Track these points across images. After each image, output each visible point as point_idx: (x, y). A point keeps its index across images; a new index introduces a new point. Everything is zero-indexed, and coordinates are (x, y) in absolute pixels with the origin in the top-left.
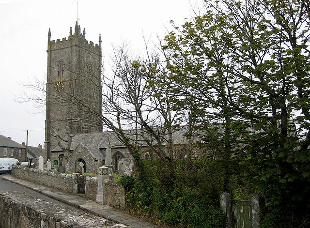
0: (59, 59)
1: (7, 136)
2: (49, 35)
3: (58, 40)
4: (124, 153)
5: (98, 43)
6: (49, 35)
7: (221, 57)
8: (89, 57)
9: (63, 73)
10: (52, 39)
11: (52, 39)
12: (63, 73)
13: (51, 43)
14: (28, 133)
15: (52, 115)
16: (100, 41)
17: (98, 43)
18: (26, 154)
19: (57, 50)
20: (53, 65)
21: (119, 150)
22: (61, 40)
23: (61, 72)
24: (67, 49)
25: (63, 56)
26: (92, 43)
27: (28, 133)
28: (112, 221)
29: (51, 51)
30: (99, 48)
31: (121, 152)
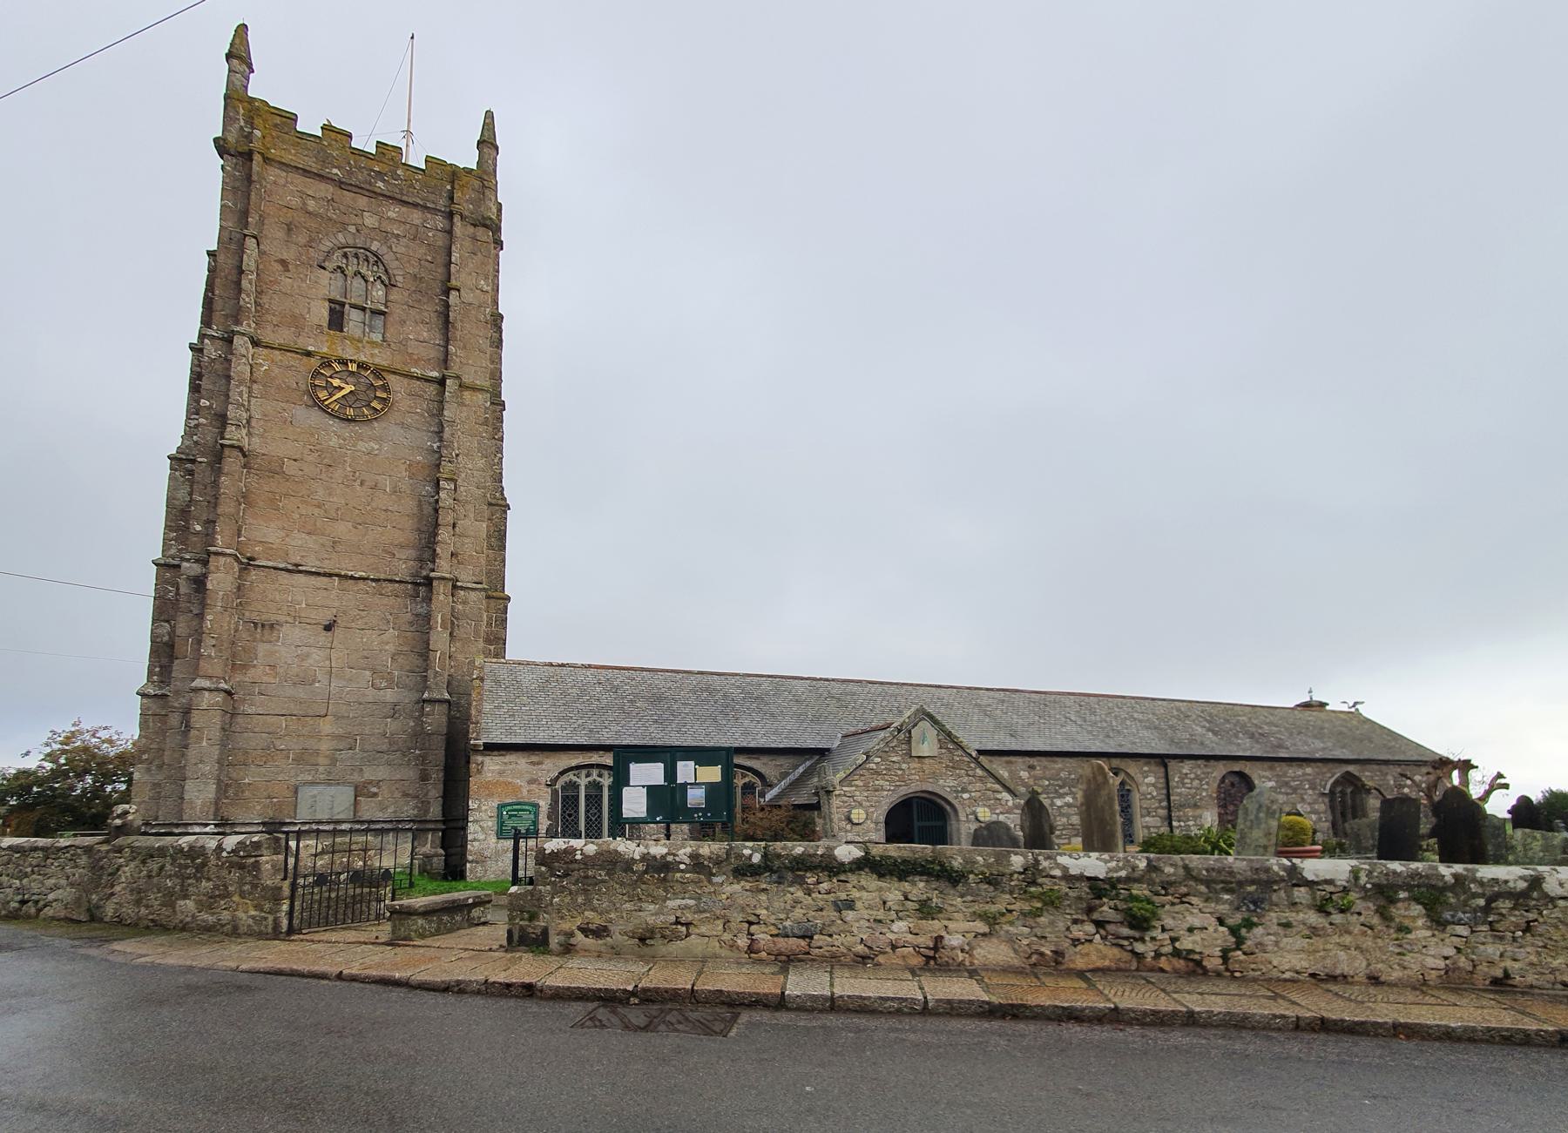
2: (239, 55)
21: (1351, 768)
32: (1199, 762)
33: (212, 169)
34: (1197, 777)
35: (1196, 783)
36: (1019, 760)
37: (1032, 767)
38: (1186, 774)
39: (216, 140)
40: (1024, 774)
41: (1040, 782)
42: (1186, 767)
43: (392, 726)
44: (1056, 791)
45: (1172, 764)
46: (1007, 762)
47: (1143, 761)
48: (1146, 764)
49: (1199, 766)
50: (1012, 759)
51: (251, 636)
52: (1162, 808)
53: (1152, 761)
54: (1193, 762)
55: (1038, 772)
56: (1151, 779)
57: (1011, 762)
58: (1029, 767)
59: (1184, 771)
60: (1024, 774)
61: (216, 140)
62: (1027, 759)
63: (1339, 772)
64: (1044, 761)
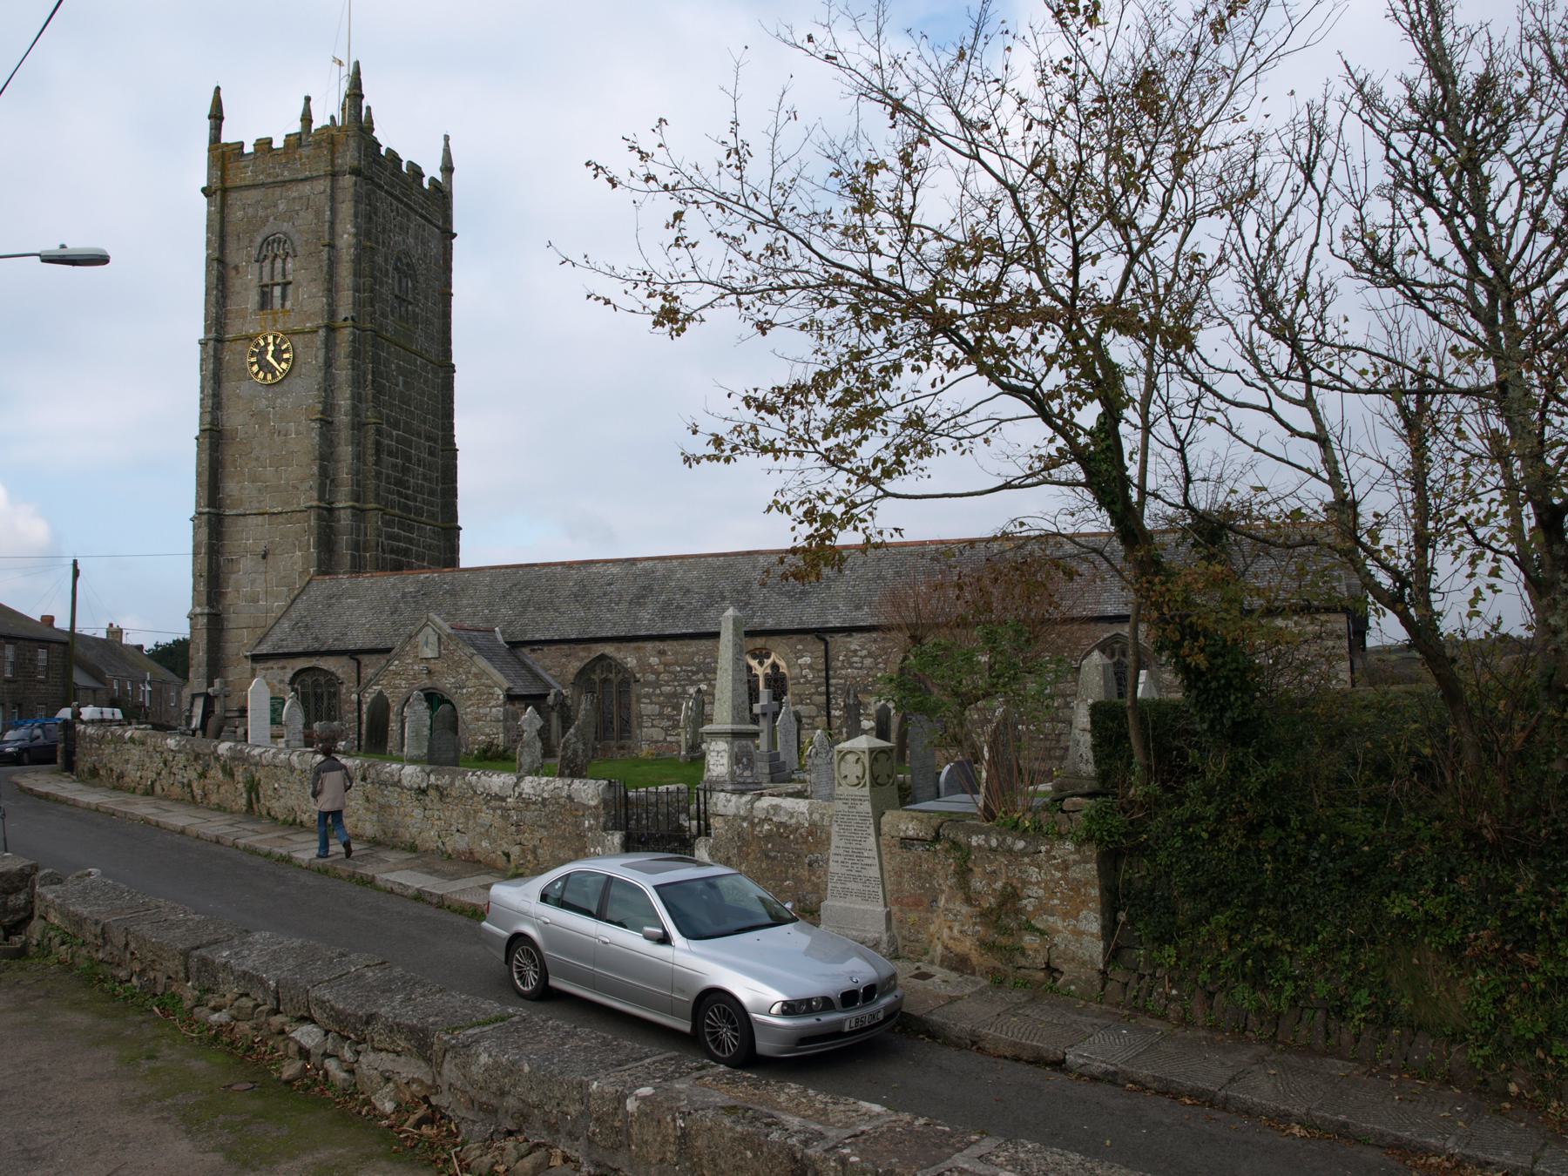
0: (267, 230)
1: (456, 359)
2: (217, 116)
3: (264, 145)
4: (631, 662)
5: (439, 177)
6: (217, 116)
7: (648, 696)
8: (404, 230)
9: (284, 297)
10: (227, 137)
11: (227, 137)
12: (284, 297)
13: (223, 156)
14: (76, 573)
15: (231, 487)
16: (448, 169)
17: (439, 177)
18: (68, 675)
19: (254, 186)
20: (235, 256)
21: (608, 650)
22: (248, 149)
23: (277, 291)
24: (306, 188)
25: (290, 216)
26: (416, 172)
27: (76, 573)
28: (386, 1173)
29: (225, 191)
30: (441, 195)
31: (619, 656)
32: (270, 664)
33: (200, 207)
34: (870, 654)
35: (868, 661)
36: (649, 645)
37: (662, 653)
38: (855, 651)
39: (204, 190)
40: (654, 660)
41: (671, 669)
42: (855, 642)
43: (1459, 59)
44: (689, 677)
45: (365, 659)
46: (635, 648)
47: (795, 638)
48: (800, 641)
49: (875, 641)
50: (640, 644)
51: (239, 1008)
52: (820, 694)
53: (809, 637)
54: (866, 635)
55: (670, 658)
56: (807, 660)
57: (639, 648)
58: (659, 652)
59: (853, 647)
60: (654, 660)
61: (204, 190)
62: (657, 644)
63: (585, 655)
64: (676, 645)
